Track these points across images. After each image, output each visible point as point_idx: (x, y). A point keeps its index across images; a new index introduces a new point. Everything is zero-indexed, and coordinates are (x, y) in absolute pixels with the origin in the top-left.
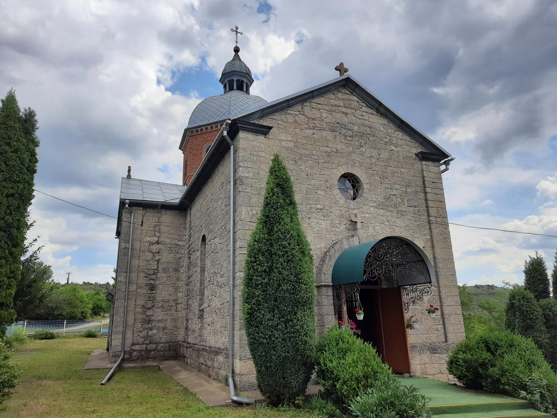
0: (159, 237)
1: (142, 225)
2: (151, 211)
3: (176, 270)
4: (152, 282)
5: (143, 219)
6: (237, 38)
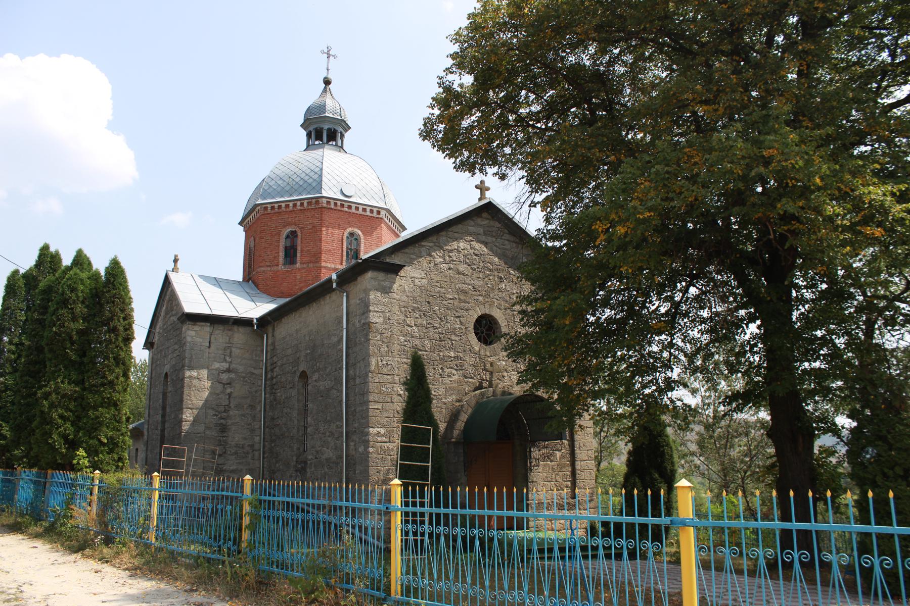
0: (231, 362)
1: (209, 347)
2: (221, 327)
3: (252, 407)
4: (222, 421)
5: (210, 338)
6: (328, 63)
